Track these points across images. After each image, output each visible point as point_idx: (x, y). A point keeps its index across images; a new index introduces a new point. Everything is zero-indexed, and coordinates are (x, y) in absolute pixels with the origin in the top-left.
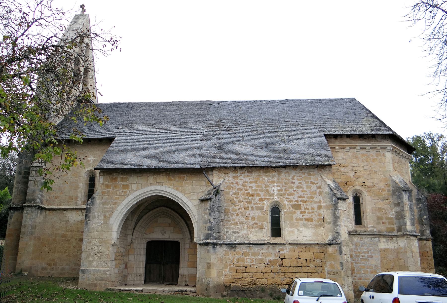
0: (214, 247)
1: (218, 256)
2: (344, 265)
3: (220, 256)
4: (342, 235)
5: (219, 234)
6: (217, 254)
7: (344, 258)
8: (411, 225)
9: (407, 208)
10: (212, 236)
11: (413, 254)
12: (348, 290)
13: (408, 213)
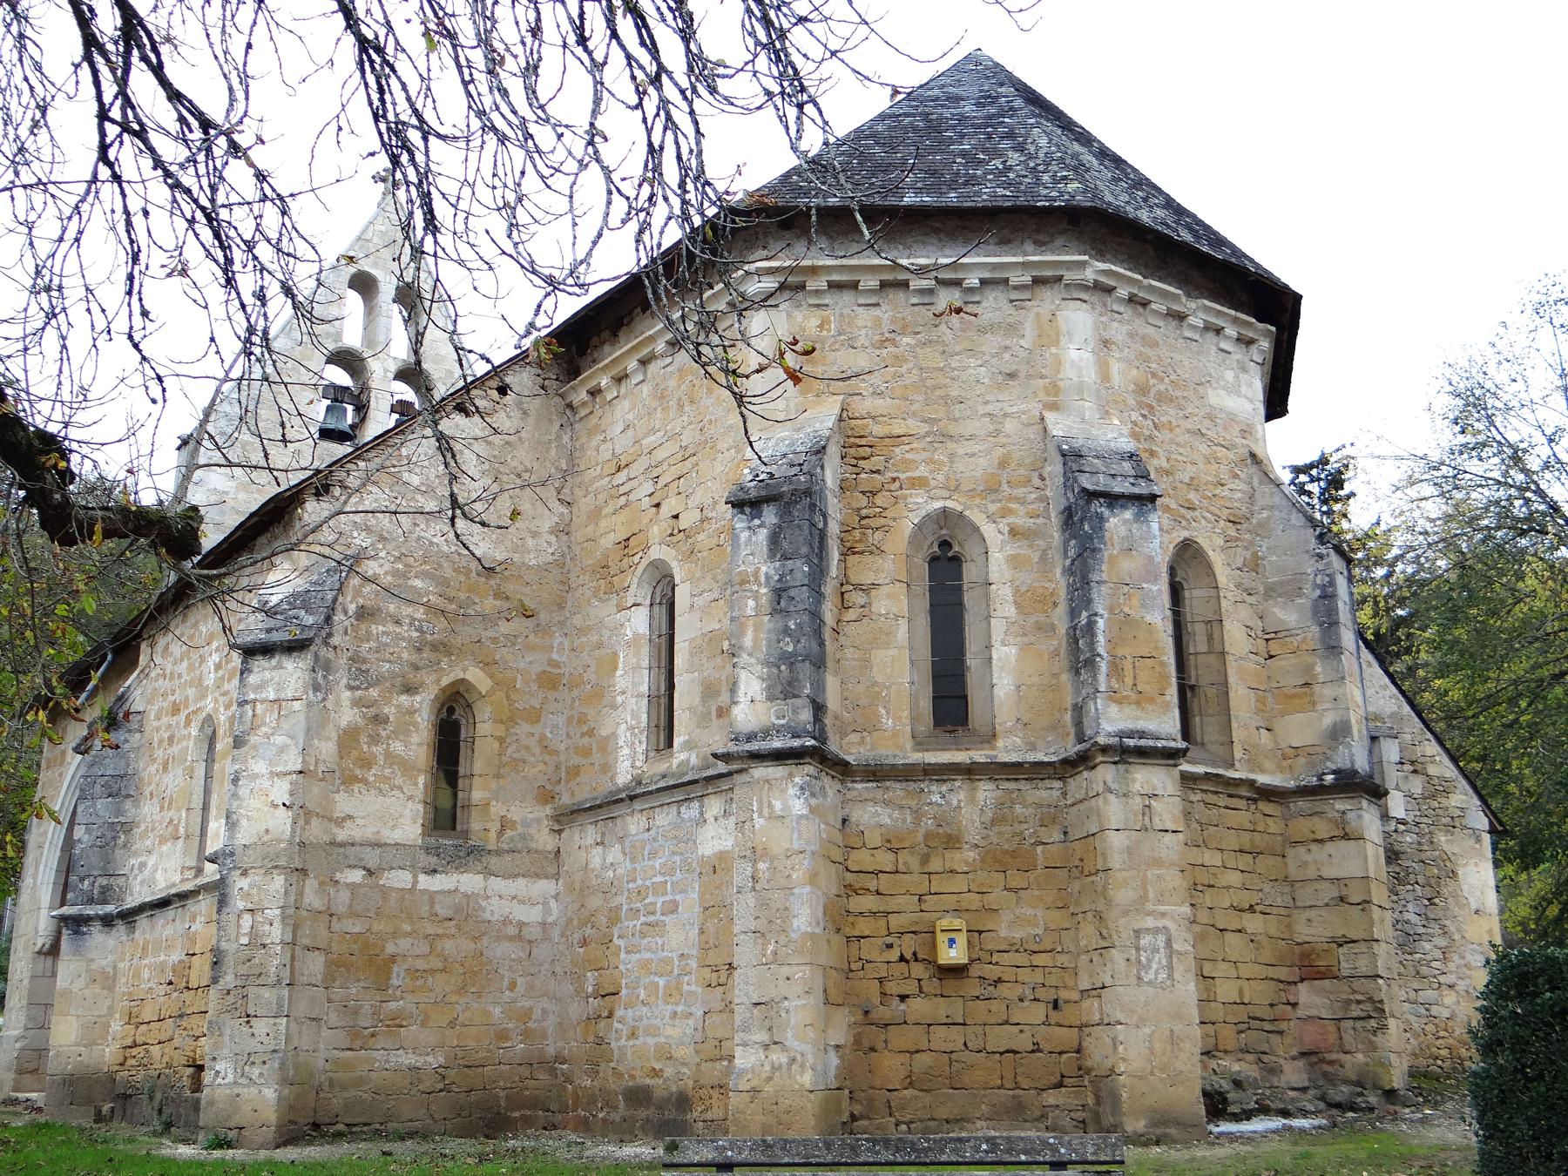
0: (77, 932)
1: (94, 966)
2: (229, 962)
3: (103, 963)
4: (244, 822)
5: (105, 882)
6: (90, 956)
7: (239, 926)
8: (771, 698)
9: (751, 603)
10: (74, 891)
11: (762, 866)
12: (235, 1083)
13: (757, 629)
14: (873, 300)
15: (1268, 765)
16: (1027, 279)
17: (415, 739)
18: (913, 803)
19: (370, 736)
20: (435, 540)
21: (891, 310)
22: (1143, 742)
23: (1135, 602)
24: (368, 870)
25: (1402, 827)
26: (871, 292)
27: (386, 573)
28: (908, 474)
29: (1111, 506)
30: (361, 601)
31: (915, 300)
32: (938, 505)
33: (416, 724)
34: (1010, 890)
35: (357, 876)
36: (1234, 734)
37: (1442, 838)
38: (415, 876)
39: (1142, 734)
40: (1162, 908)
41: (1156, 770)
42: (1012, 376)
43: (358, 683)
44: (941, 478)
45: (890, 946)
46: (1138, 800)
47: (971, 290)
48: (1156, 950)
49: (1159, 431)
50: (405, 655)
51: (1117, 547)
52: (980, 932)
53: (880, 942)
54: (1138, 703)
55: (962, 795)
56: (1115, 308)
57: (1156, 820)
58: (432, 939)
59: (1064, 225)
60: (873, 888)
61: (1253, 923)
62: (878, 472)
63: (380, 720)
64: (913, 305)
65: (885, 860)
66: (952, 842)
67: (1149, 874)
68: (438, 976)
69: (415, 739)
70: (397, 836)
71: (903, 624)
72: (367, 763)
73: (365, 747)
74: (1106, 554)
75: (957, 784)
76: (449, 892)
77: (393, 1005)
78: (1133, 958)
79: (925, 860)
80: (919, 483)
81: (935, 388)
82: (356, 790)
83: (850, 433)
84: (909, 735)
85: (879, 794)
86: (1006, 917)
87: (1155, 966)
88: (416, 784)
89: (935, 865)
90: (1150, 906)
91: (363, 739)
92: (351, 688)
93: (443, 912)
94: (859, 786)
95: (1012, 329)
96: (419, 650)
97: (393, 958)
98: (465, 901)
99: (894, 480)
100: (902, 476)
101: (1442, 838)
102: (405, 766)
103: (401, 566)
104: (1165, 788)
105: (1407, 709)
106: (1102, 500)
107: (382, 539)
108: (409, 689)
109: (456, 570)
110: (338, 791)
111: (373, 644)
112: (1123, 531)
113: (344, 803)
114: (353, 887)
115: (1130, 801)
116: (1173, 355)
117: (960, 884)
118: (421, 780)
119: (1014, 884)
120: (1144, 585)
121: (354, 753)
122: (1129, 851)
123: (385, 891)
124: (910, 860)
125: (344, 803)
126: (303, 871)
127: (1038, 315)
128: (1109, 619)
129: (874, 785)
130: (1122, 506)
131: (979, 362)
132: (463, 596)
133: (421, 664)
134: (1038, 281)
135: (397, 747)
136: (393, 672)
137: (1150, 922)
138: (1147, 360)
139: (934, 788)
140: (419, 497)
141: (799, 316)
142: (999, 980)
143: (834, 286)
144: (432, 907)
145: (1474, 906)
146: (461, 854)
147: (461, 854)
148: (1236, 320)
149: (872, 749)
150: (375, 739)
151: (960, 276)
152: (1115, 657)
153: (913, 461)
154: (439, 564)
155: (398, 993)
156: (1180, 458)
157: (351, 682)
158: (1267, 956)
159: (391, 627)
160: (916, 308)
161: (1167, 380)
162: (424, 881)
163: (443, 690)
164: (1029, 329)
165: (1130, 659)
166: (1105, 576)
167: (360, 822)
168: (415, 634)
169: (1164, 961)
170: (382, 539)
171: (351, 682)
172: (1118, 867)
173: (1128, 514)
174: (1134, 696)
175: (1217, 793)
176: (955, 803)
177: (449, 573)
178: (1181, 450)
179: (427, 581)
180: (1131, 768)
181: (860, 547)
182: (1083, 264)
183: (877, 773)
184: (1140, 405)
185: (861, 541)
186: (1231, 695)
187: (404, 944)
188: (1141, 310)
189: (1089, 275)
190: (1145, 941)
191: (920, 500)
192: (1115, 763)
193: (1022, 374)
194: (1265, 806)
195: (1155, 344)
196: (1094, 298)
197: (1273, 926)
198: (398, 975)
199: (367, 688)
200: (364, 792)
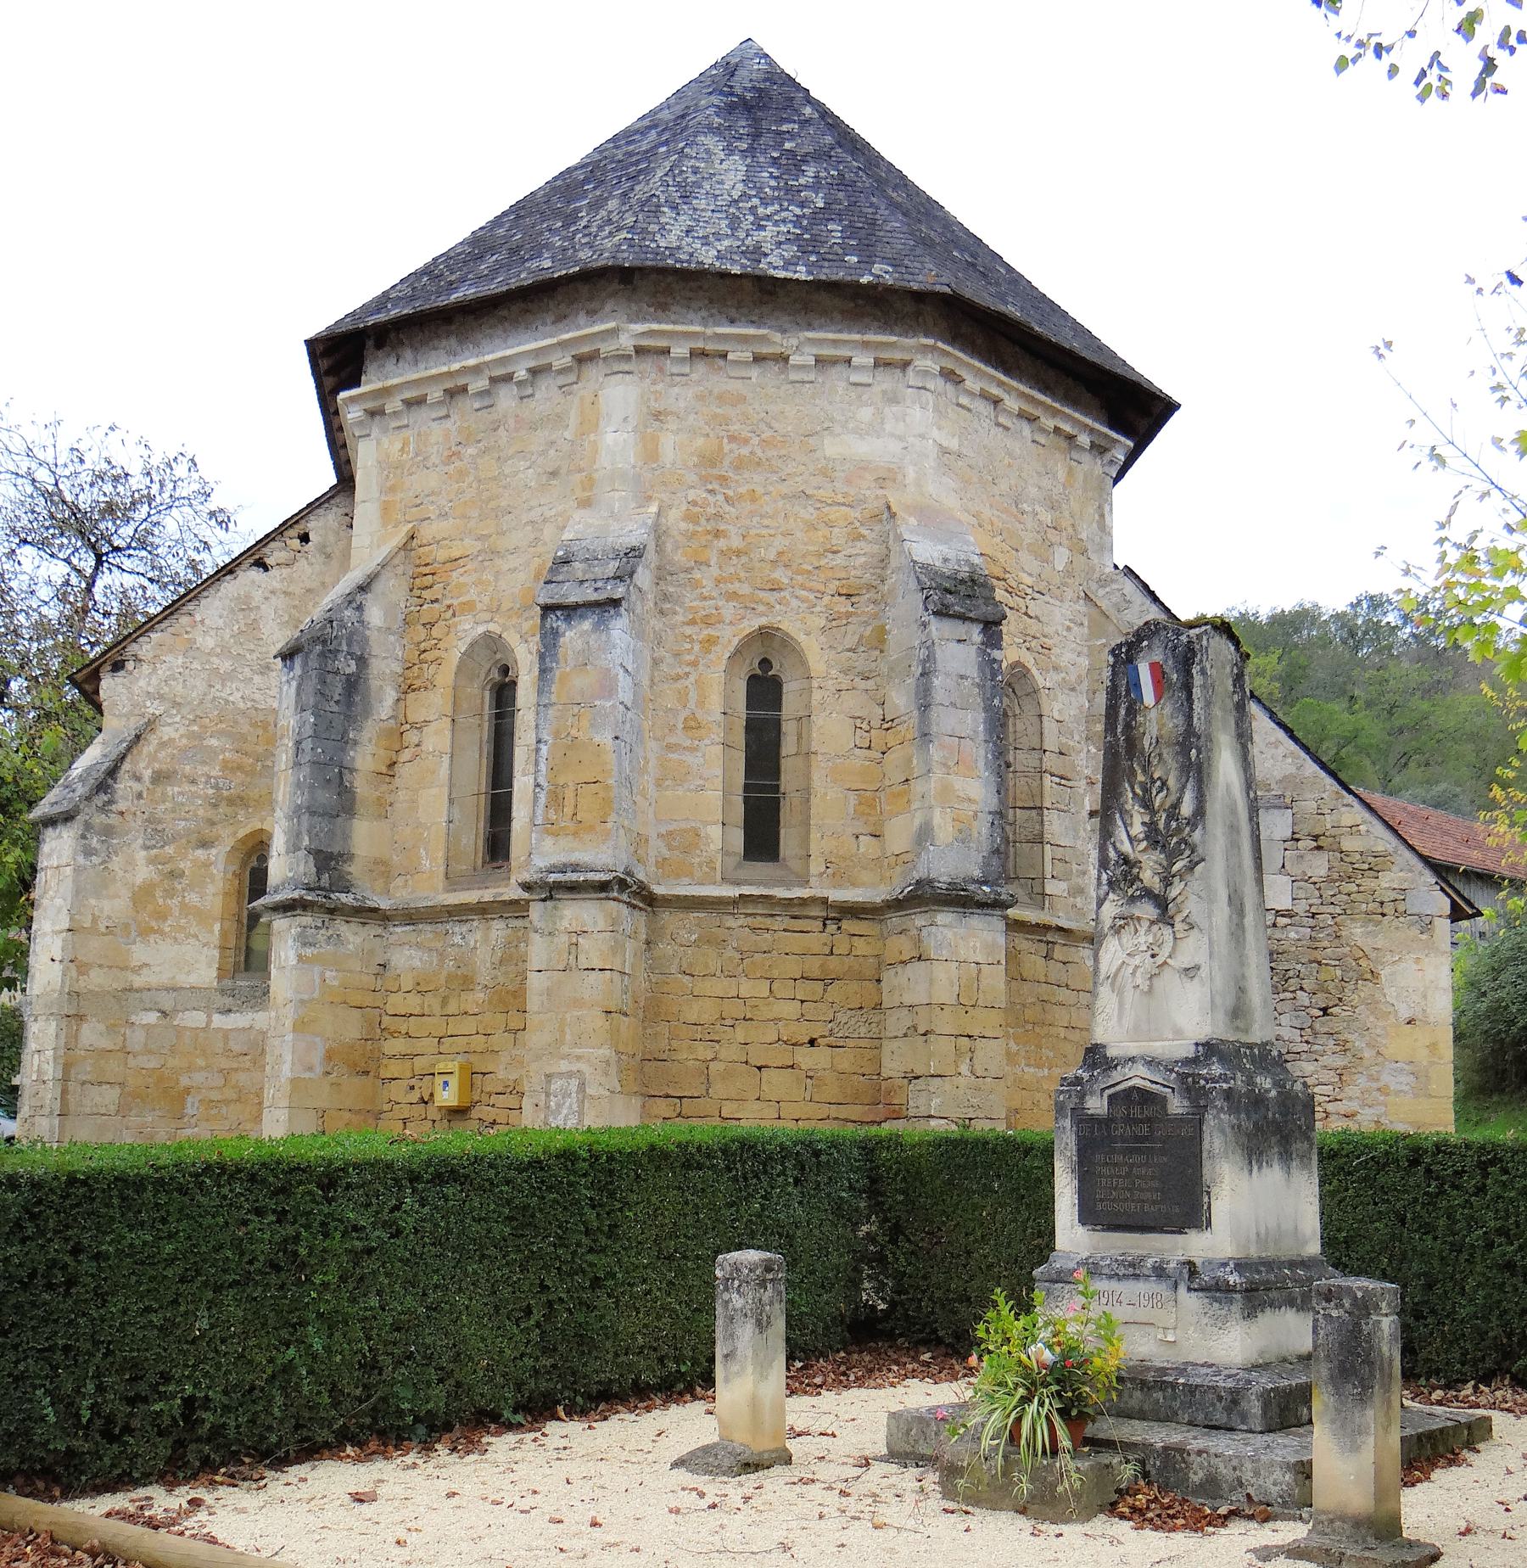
4: (37, 975)
14: (443, 412)
15: (866, 876)
16: (567, 360)
17: (211, 889)
18: (439, 945)
19: (165, 890)
20: (231, 698)
21: (465, 413)
22: (574, 877)
23: (585, 723)
24: (163, 1012)
25: (1282, 921)
26: (682, 360)
27: (182, 736)
28: (461, 599)
29: (568, 619)
30: (157, 766)
31: (477, 405)
32: (481, 629)
33: (212, 876)
34: (509, 1031)
35: (152, 1018)
36: (813, 846)
37: (1356, 932)
38: (209, 1016)
39: (576, 868)
40: (578, 1051)
41: (589, 904)
42: (554, 474)
43: (154, 842)
44: (486, 600)
45: (412, 1088)
46: (564, 938)
47: (520, 384)
48: (568, 1095)
49: (733, 505)
50: (201, 812)
51: (571, 663)
52: (484, 1074)
53: (405, 1083)
54: (575, 834)
55: (478, 935)
56: (675, 370)
57: (582, 958)
58: (226, 1073)
59: (615, 286)
60: (403, 1032)
61: (807, 1058)
62: (436, 601)
63: (174, 875)
64: (477, 410)
65: (413, 1003)
66: (467, 983)
67: (568, 1016)
68: (232, 1106)
69: (211, 889)
70: (193, 980)
71: (446, 759)
72: (162, 916)
73: (161, 901)
74: (557, 673)
75: (475, 924)
76: (244, 1029)
77: (189, 1132)
78: (542, 1104)
79: (445, 1002)
80: (469, 607)
81: (490, 499)
82: (152, 941)
83: (418, 562)
84: (442, 876)
85: (413, 938)
86: (504, 1058)
87: (565, 1111)
88: (212, 932)
89: (452, 1008)
90: (565, 1049)
91: (159, 893)
92: (146, 848)
93: (237, 1048)
94: (398, 930)
95: (559, 420)
96: (215, 806)
97: (187, 1091)
98: (260, 1038)
99: (449, 607)
100: (455, 602)
101: (1356, 932)
102: (201, 916)
103: (196, 728)
104: (595, 923)
105: (1312, 768)
106: (559, 613)
107: (176, 704)
108: (205, 844)
109: (252, 725)
110: (134, 943)
111: (168, 805)
112: (579, 644)
113: (139, 953)
114: (148, 1027)
115: (556, 940)
116: (768, 408)
117: (469, 1026)
118: (217, 927)
119: (512, 1025)
120: (597, 703)
121: (150, 907)
122: (549, 992)
123: (179, 1031)
124: (432, 1002)
125: (139, 953)
126: (80, 1017)
127: (582, 398)
128: (554, 744)
129: (412, 927)
130: (581, 616)
131: (528, 463)
132: (260, 749)
133: (216, 819)
134: (581, 360)
135: (193, 898)
136: (189, 829)
137: (564, 1066)
138: (726, 421)
139: (457, 929)
140: (214, 659)
141: (385, 441)
142: (494, 1123)
143: (409, 403)
144: (226, 1043)
145: (1405, 1014)
146: (257, 994)
147: (257, 994)
148: (866, 345)
149: (412, 892)
150: (170, 893)
151: (510, 370)
152: (556, 786)
153: (465, 585)
154: (236, 722)
155: (193, 1121)
156: (764, 532)
157: (147, 842)
158: (831, 1091)
159: (187, 787)
160: (479, 413)
161: (756, 440)
162: (218, 1021)
163: (243, 841)
164: (573, 419)
165: (572, 788)
166: (554, 698)
167: (157, 969)
168: (211, 791)
169: (575, 1107)
170: (176, 704)
171: (147, 842)
172: (536, 1009)
173: (587, 625)
174: (571, 826)
175: (772, 915)
176: (472, 943)
177: (245, 728)
178: (766, 522)
179: (223, 739)
180: (560, 905)
181: (417, 683)
182: (614, 332)
183: (411, 917)
184: (705, 480)
185: (418, 677)
186: (815, 801)
187: (199, 1078)
188: (721, 362)
189: (626, 342)
190: (556, 1085)
191: (467, 627)
192: (544, 900)
193: (563, 471)
194: (848, 925)
195: (742, 399)
196: (648, 365)
197: (845, 1060)
198: (193, 1106)
199: (163, 846)
200: (160, 942)
